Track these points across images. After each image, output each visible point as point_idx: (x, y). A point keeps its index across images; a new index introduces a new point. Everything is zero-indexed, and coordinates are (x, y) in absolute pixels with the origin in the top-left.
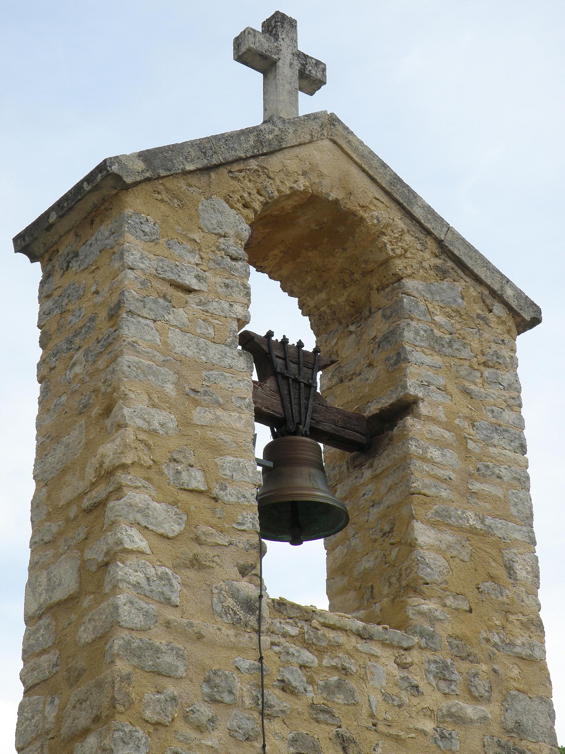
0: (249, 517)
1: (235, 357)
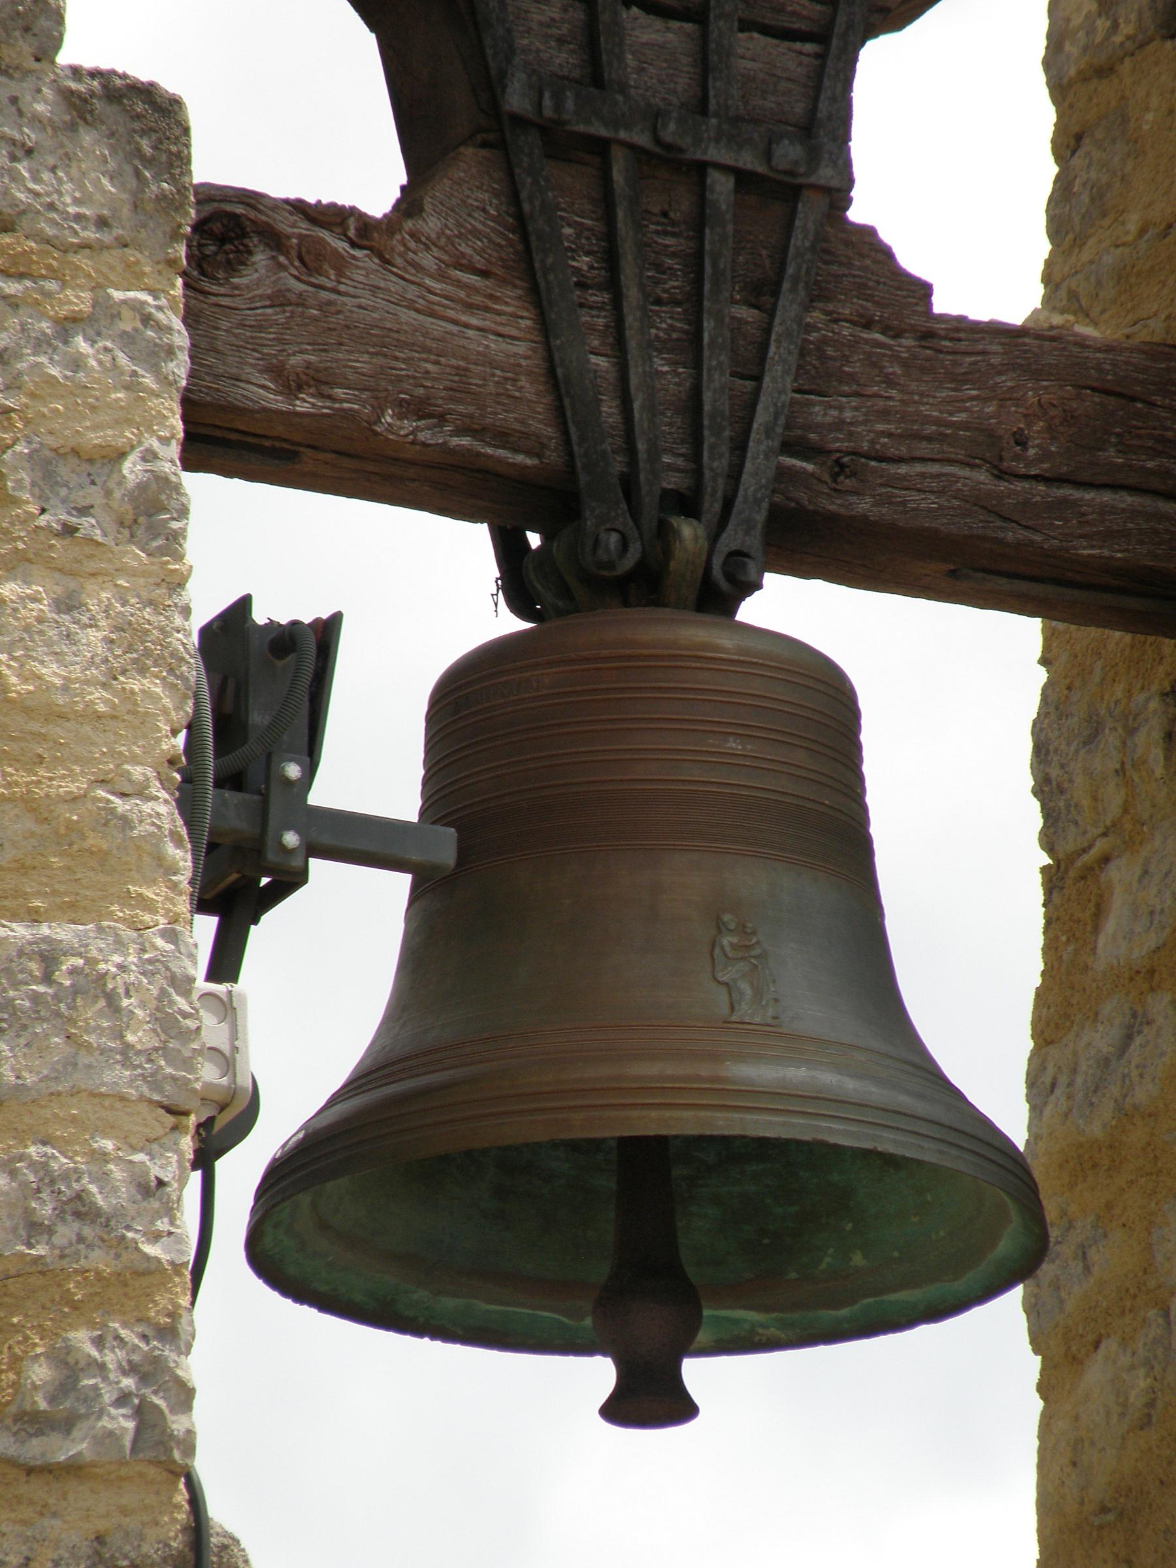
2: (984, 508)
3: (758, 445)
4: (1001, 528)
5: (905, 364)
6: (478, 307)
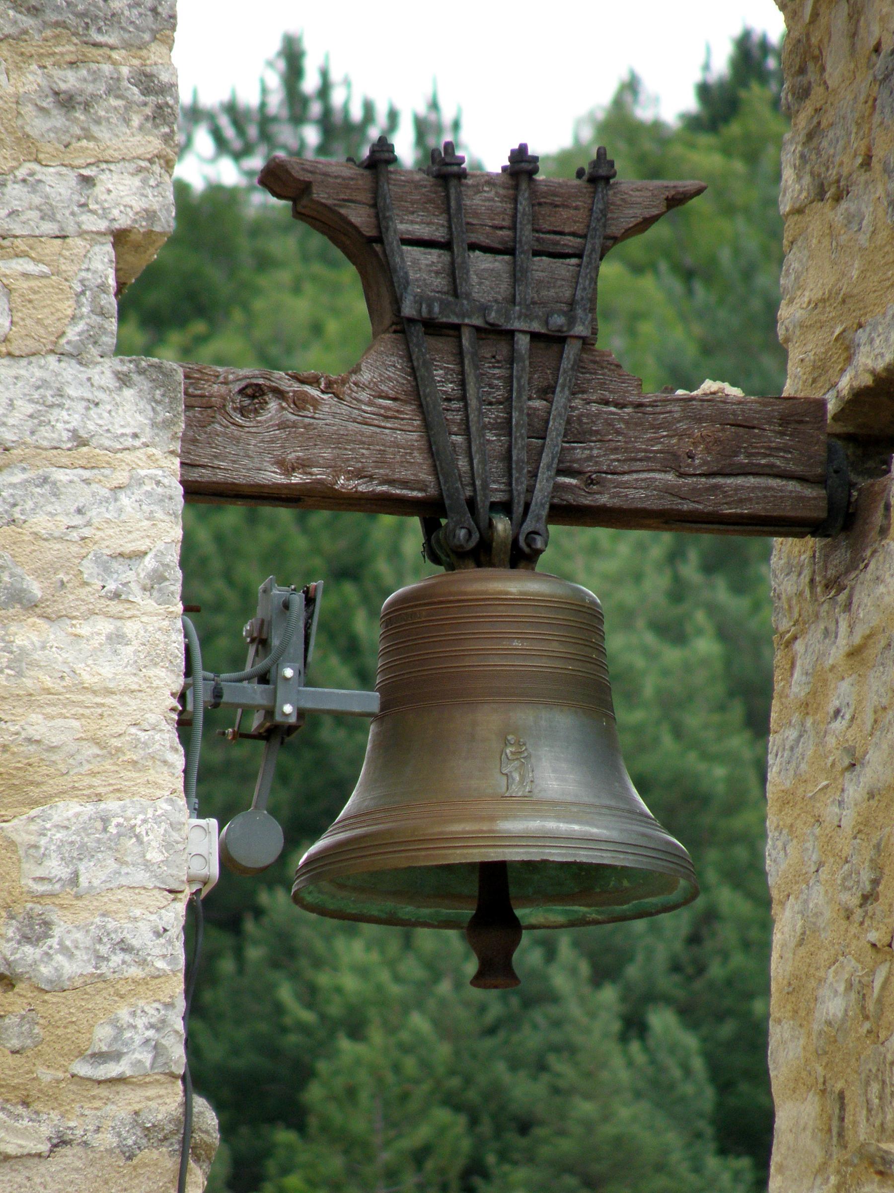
0: (140, 1022)
1: (100, 395)
2: (671, 494)
3: (543, 474)
4: (680, 504)
5: (627, 423)
6: (391, 418)
